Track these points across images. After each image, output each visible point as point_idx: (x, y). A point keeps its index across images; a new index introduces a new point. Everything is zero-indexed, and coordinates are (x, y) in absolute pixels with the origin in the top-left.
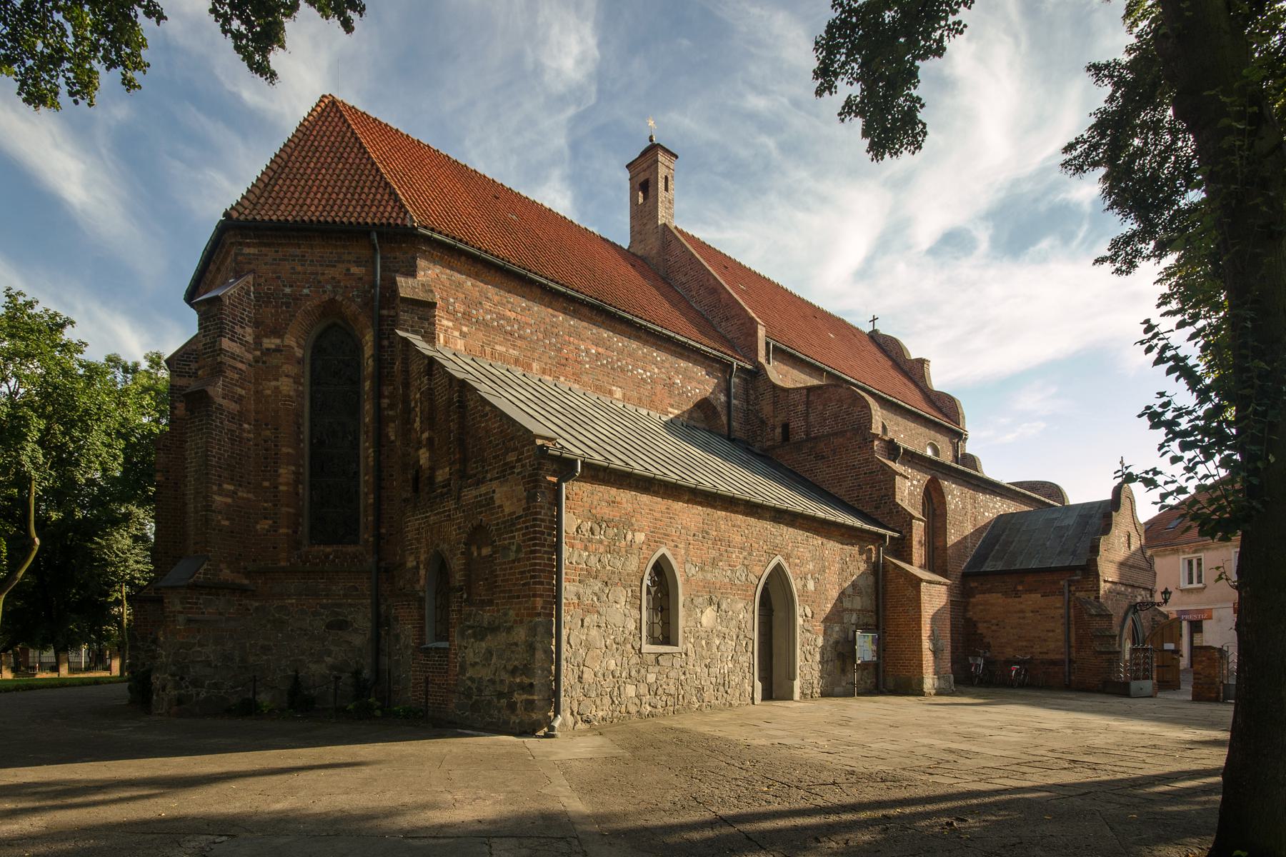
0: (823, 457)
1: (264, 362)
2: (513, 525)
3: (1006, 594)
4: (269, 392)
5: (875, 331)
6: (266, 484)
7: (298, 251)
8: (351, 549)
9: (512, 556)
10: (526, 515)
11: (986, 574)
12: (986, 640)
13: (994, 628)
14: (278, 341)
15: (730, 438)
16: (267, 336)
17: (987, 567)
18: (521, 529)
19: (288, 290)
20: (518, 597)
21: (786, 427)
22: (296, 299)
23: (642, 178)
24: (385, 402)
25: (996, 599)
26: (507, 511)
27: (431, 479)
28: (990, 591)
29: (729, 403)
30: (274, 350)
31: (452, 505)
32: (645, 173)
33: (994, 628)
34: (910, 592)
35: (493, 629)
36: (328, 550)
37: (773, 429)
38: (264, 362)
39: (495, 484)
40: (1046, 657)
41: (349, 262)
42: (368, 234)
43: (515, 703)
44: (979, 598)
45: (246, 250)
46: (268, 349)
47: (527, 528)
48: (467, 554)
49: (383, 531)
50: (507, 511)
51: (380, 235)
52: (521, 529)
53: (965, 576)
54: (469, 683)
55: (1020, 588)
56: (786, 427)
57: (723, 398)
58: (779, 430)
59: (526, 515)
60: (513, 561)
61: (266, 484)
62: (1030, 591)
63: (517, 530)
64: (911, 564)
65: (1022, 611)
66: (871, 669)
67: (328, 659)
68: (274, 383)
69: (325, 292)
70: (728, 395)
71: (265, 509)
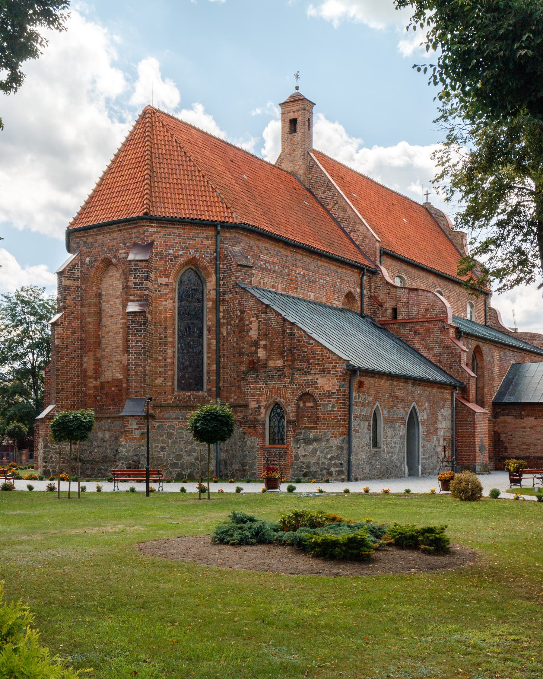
0: (419, 334)
1: (159, 291)
2: (331, 396)
3: (516, 417)
4: (162, 308)
5: (427, 203)
6: (161, 358)
7: (176, 231)
8: (200, 393)
9: (330, 409)
10: (338, 392)
11: (505, 404)
12: (505, 445)
13: (510, 437)
14: (167, 280)
15: (362, 315)
16: (160, 277)
17: (506, 400)
18: (335, 398)
19: (171, 252)
20: (333, 427)
21: (395, 310)
22: (175, 257)
23: (292, 116)
24: (221, 315)
25: (510, 419)
26: (326, 389)
27: (266, 365)
28: (508, 415)
29: (362, 292)
30: (165, 285)
31: (287, 381)
32: (297, 117)
33: (510, 437)
34: (470, 419)
35: (316, 440)
36: (189, 394)
37: (386, 309)
38: (159, 291)
39: (318, 376)
40: (536, 455)
41: (203, 238)
42: (216, 226)
43: (332, 472)
44: (502, 418)
45: (150, 229)
46: (161, 284)
47: (338, 398)
48: (297, 405)
49: (220, 385)
50: (326, 389)
51: (222, 227)
52: (335, 398)
53: (495, 405)
54: (302, 464)
55: (523, 413)
56: (395, 310)
57: (358, 290)
58: (390, 311)
59: (338, 392)
60: (331, 411)
61: (161, 358)
62: (528, 416)
63: (332, 398)
64: (469, 402)
65: (524, 428)
66: (353, 476)
67: (194, 454)
68: (164, 303)
69: (190, 253)
70: (361, 288)
71: (160, 372)
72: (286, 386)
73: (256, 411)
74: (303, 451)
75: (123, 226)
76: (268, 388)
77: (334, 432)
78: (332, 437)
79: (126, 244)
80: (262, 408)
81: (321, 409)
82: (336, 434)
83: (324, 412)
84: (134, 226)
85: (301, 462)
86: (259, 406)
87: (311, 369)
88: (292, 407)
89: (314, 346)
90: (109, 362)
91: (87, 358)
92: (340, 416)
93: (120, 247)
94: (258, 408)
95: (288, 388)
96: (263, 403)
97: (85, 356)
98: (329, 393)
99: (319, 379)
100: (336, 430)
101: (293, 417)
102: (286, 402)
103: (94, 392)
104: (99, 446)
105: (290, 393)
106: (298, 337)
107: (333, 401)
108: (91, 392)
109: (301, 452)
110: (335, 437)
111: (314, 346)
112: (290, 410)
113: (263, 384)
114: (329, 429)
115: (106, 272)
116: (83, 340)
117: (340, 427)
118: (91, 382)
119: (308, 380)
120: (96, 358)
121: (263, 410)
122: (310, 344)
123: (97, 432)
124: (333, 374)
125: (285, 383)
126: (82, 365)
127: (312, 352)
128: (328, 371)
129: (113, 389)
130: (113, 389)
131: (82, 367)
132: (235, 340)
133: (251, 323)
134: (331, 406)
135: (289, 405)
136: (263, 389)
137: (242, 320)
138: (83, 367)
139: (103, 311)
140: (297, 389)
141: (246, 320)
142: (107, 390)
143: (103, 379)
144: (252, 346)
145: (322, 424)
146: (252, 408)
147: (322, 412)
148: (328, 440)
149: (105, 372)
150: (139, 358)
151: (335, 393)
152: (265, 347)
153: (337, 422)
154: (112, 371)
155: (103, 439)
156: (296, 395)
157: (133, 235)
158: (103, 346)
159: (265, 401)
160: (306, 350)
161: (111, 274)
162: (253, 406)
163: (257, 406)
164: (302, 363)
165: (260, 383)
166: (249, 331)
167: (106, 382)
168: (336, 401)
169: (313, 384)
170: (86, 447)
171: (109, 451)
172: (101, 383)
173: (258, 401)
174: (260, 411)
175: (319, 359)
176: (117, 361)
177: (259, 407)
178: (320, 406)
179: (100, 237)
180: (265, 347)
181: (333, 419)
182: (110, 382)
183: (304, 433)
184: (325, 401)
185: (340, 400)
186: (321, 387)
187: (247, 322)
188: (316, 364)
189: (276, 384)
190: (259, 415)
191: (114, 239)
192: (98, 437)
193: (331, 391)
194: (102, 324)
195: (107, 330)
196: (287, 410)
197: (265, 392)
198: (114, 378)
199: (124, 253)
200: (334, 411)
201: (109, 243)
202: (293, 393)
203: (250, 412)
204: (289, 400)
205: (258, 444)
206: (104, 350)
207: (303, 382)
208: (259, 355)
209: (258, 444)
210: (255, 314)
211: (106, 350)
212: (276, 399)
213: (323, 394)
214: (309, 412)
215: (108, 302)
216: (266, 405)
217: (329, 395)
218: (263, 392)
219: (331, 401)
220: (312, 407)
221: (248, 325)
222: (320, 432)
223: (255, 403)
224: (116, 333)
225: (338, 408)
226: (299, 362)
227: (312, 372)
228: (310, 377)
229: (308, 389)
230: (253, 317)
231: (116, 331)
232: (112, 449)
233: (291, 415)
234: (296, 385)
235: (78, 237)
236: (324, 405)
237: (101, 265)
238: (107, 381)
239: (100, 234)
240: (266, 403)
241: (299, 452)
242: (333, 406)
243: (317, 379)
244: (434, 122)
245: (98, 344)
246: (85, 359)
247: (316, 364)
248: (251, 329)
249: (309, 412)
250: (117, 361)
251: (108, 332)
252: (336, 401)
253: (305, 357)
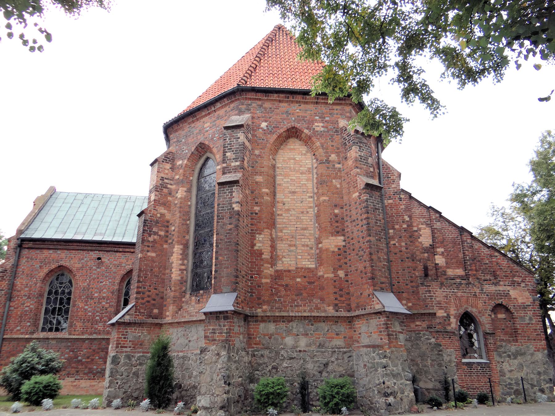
2: (526, 308)
18: (531, 311)
20: (535, 340)
60: (529, 324)
72: (476, 295)
73: (445, 320)
74: (508, 366)
75: (323, 99)
76: (457, 297)
77: (537, 345)
78: (535, 351)
79: (324, 118)
80: (452, 317)
81: (518, 321)
82: (539, 348)
83: (522, 324)
84: (338, 102)
85: (509, 378)
86: (448, 315)
87: (500, 281)
88: (486, 318)
89: (499, 259)
90: (290, 246)
91: (261, 236)
92: (539, 329)
93: (316, 120)
94: (447, 317)
95: (480, 298)
96: (453, 312)
97: (260, 234)
98: (524, 306)
99: (511, 291)
100: (538, 344)
101: (489, 329)
102: (480, 313)
103: (271, 281)
104: (291, 358)
105: (482, 303)
106: (476, 249)
107: (530, 314)
108: (268, 281)
109: (506, 367)
110: (538, 351)
111: (499, 259)
112: (485, 320)
113: (450, 292)
114: (531, 342)
115: (285, 143)
116: (256, 214)
117: (541, 340)
118: (268, 269)
119: (500, 291)
120: (272, 240)
121: (453, 320)
122: (494, 256)
123: (283, 338)
124: (523, 287)
125: (475, 293)
126: (253, 245)
127: (497, 264)
128: (518, 283)
129: (298, 280)
130: (298, 280)
131: (252, 247)
132: (403, 244)
133: (420, 229)
134: (528, 318)
135: (484, 315)
136: (450, 297)
137: (410, 225)
138: (256, 248)
139: (280, 185)
140: (490, 299)
141: (415, 226)
142: (286, 280)
143: (280, 266)
144: (424, 253)
145: (522, 337)
146: (439, 317)
147: (519, 324)
148: (532, 355)
149: (283, 257)
150: (380, 240)
151: (530, 305)
152: (442, 254)
153: (537, 335)
154: (296, 258)
155: (294, 347)
156: (489, 305)
157: (335, 112)
158: (278, 226)
159: (454, 310)
160: (487, 262)
161: (292, 147)
162: (441, 315)
163: (445, 315)
164: (485, 274)
165: (446, 290)
166: (419, 238)
167: (285, 271)
168: (533, 313)
169: (506, 296)
170: (266, 360)
171: (310, 366)
172: (277, 271)
173: (446, 310)
174: (449, 320)
175: (506, 271)
176: (303, 246)
177: (448, 316)
178: (517, 318)
179: (286, 105)
180: (442, 254)
181: (532, 332)
182: (293, 270)
183: (505, 346)
184: (521, 313)
185: (536, 313)
186: (514, 299)
187: (415, 229)
188: (504, 276)
189: (465, 292)
190: (449, 324)
191: (306, 110)
192: (285, 345)
193: (525, 303)
194: (277, 200)
195: (287, 208)
196: (481, 320)
197: (453, 301)
198: (299, 266)
199: (323, 127)
200: (532, 324)
201: (298, 112)
202: (485, 303)
203: (438, 321)
204: (482, 310)
205: (456, 358)
206: (281, 231)
207: (495, 293)
208: (437, 262)
209: (456, 358)
210: (424, 222)
211: (284, 231)
212: (467, 308)
213: (517, 306)
214: (502, 324)
215: (286, 176)
216: (456, 314)
217: (524, 307)
218: (450, 300)
219: (527, 313)
220: (505, 319)
221: (416, 231)
222: (522, 345)
223: (443, 311)
224: (302, 212)
225: (536, 321)
226: (482, 273)
227: (501, 283)
228: (501, 288)
229: (501, 300)
230: (422, 224)
231: (302, 210)
232: (317, 362)
233: (487, 326)
234: (487, 295)
235: (250, 99)
236: (521, 317)
237: (284, 134)
238: (286, 269)
239: (287, 102)
240: (456, 312)
241: (504, 367)
242: (531, 319)
243: (509, 291)
244: (541, 100)
245: (272, 224)
246: (259, 237)
247: (504, 276)
248: (421, 235)
249: (502, 324)
250: (303, 246)
251: (289, 210)
252: (533, 313)
253: (487, 268)
